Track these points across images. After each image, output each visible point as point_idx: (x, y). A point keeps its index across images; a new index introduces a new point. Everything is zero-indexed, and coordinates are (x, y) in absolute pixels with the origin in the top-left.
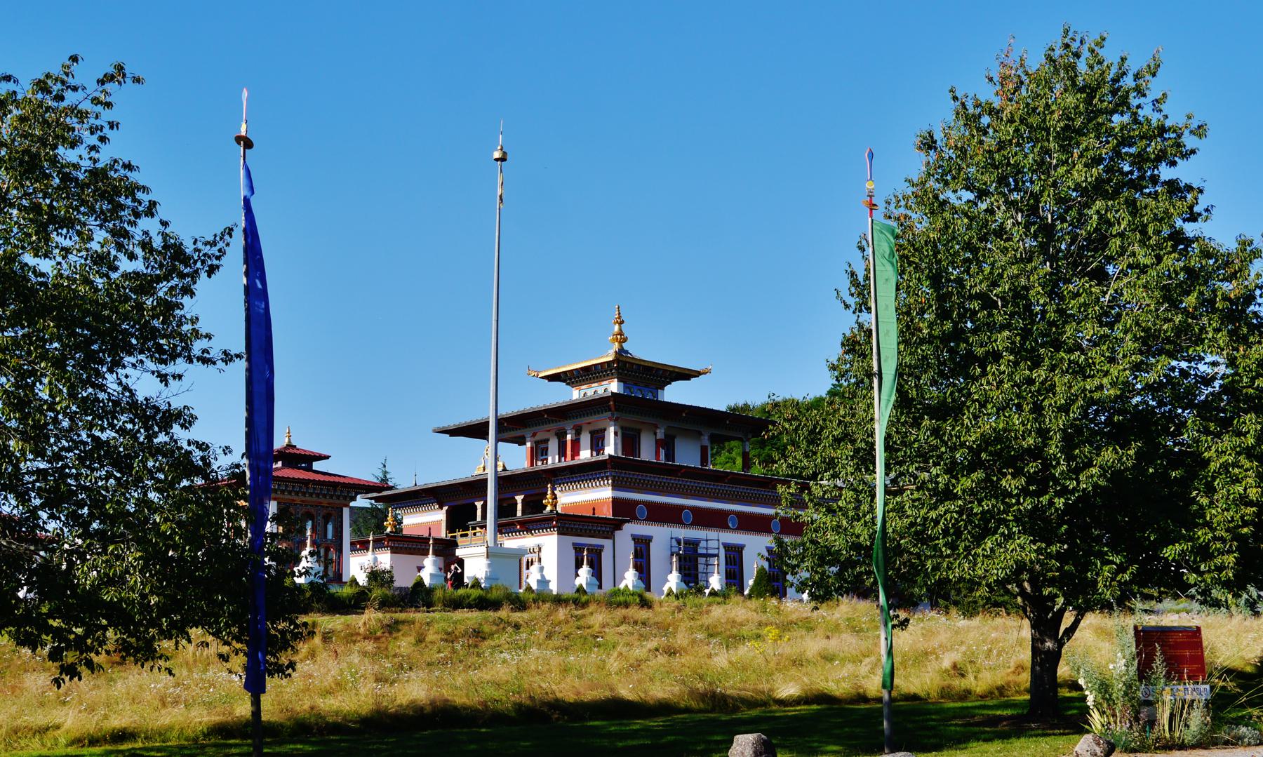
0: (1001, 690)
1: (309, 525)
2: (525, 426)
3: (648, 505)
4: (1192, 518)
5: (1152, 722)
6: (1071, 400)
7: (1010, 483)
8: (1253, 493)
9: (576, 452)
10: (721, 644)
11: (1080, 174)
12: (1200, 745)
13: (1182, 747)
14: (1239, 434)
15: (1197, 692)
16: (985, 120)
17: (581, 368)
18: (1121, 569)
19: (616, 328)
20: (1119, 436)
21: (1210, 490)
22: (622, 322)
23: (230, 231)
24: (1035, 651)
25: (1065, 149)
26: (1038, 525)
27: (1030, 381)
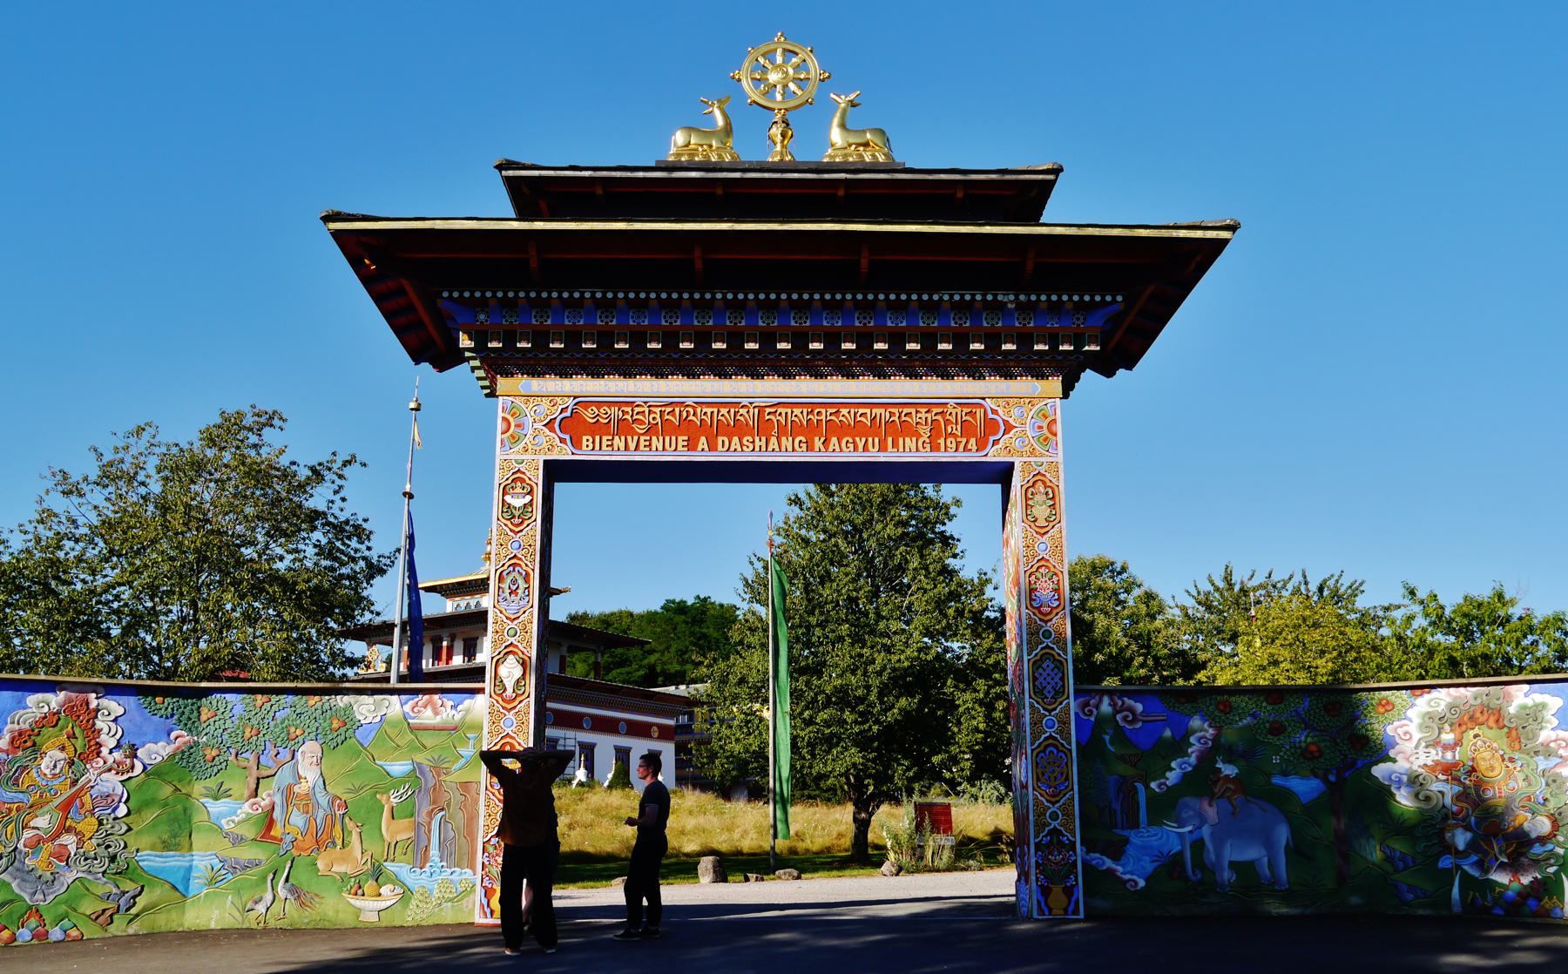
0: (829, 849)
3: (592, 717)
4: (947, 740)
5: (922, 858)
6: (884, 668)
7: (848, 716)
8: (982, 726)
9: (449, 658)
11: (891, 530)
12: (948, 870)
13: (938, 871)
14: (976, 691)
15: (947, 841)
18: (909, 769)
20: (908, 691)
21: (959, 723)
23: (398, 550)
24: (855, 820)
25: (883, 514)
26: (862, 742)
27: (861, 656)
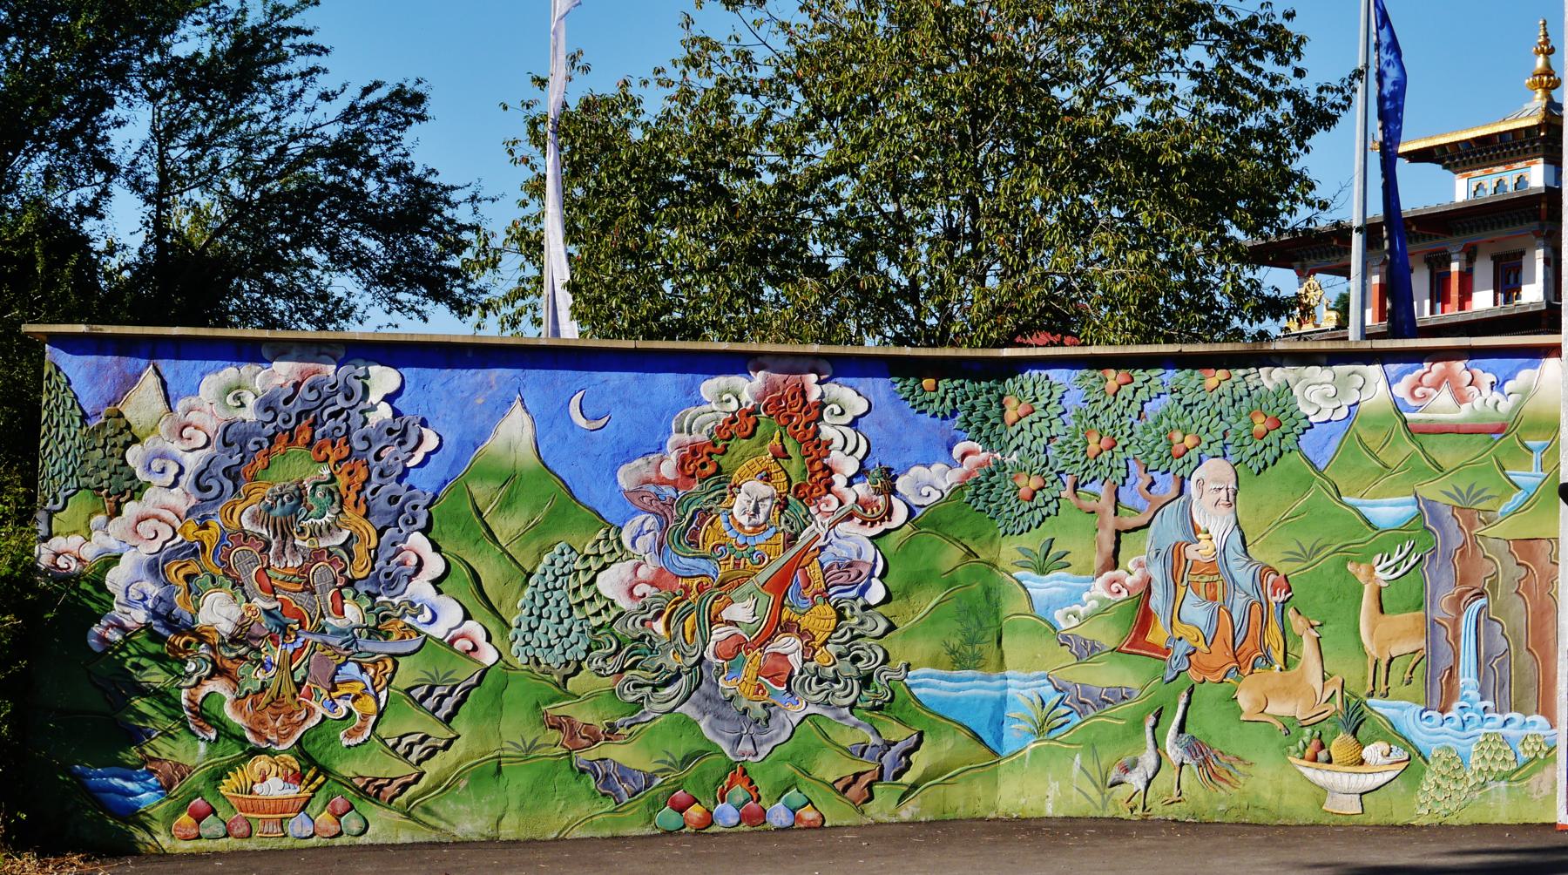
1: (26, 328)
2: (1449, 232)
9: (1466, 296)
10: (346, 316)
16: (783, 299)
17: (1477, 140)
19: (1540, 62)
22: (1551, 51)
